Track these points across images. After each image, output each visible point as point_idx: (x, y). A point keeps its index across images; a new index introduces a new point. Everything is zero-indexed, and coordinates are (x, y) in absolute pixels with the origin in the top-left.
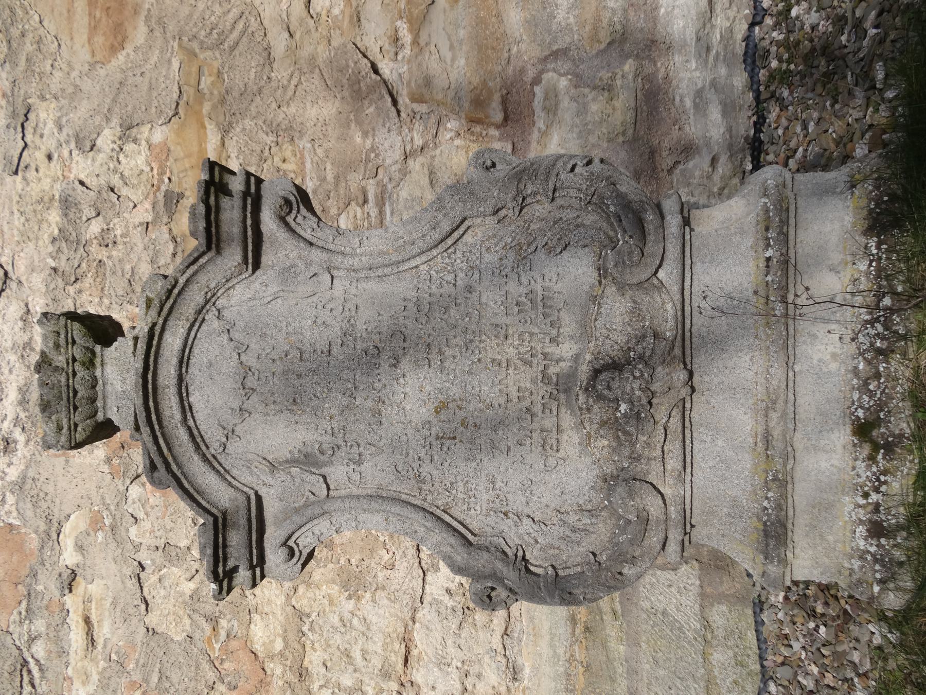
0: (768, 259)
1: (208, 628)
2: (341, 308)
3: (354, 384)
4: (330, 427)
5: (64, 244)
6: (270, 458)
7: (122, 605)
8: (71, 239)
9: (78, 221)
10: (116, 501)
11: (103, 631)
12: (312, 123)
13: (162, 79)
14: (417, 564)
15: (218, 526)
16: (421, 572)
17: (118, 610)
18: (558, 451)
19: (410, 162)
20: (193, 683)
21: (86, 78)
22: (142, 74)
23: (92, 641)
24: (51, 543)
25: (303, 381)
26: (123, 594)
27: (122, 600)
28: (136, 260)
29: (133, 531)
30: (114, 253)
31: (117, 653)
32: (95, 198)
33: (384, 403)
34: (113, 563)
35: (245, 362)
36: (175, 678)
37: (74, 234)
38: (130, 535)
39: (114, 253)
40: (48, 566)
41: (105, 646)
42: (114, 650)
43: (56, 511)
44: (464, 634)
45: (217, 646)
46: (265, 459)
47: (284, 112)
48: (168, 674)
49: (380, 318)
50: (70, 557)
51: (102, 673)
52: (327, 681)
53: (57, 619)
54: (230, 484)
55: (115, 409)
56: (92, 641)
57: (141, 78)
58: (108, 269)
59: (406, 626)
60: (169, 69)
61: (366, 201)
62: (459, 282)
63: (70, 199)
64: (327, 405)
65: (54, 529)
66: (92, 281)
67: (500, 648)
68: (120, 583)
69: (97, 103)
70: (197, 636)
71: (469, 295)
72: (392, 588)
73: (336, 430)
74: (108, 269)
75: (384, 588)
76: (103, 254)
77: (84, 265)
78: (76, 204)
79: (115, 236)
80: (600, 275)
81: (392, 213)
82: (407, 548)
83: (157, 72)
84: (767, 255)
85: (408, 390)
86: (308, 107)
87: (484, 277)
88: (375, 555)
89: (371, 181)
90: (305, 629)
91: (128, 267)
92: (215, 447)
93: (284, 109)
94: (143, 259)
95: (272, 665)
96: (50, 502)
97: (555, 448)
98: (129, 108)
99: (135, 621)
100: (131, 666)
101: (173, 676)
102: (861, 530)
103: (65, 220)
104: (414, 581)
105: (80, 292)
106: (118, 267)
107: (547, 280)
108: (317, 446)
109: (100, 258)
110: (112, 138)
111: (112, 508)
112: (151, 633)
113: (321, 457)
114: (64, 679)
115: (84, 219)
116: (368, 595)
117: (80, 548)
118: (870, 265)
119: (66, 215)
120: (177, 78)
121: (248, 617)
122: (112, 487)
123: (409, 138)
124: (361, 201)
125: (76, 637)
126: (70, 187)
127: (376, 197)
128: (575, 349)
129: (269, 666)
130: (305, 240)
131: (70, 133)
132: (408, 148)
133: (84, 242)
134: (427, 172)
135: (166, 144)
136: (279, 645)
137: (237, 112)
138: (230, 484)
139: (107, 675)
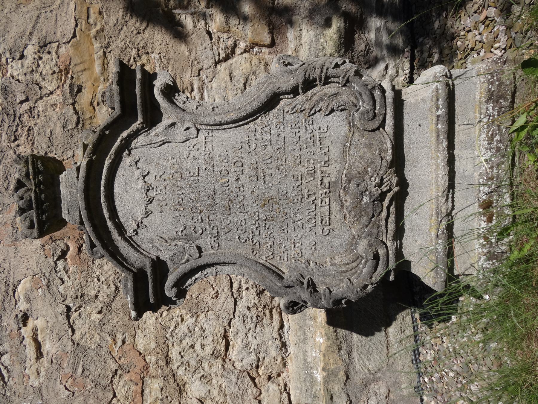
0: (438, 116)
1: (110, 339)
2: (204, 148)
3: (214, 191)
4: (200, 217)
5: (6, 117)
6: (164, 236)
7: (57, 331)
8: (10, 113)
9: (14, 102)
10: (49, 270)
11: (46, 347)
12: (159, 44)
13: (63, 15)
14: (230, 295)
15: (139, 277)
16: (233, 299)
17: (55, 333)
18: (330, 225)
19: (218, 66)
20: (103, 371)
21: (14, 13)
22: (51, 11)
23: (39, 355)
24: (9, 298)
25: (183, 191)
26: (56, 324)
27: (57, 328)
28: (53, 126)
29: (61, 288)
30: (38, 121)
31: (56, 358)
32: (24, 88)
33: (232, 202)
34: (49, 307)
35: (147, 181)
36: (92, 369)
37: (12, 111)
38: (60, 290)
39: (38, 121)
40: (8, 311)
41: (48, 355)
42: (54, 357)
43: (11, 278)
44: (258, 329)
45: (116, 350)
46: (161, 238)
47: (142, 37)
48: (88, 367)
49: (227, 153)
50: (23, 306)
51: (47, 370)
52: (182, 363)
53: (17, 341)
54: (141, 253)
55: (67, 212)
56: (39, 355)
57: (51, 14)
58: (35, 131)
59: (225, 329)
60: (68, 8)
61: (193, 90)
62: (272, 132)
63: (8, 89)
64: (198, 205)
65: (10, 289)
66: (25, 139)
67: (278, 337)
68: (55, 318)
69: (22, 29)
70: (104, 345)
71: (278, 139)
72: (217, 309)
73: (204, 219)
74: (35, 131)
75: (212, 310)
76: (31, 123)
77: (19, 129)
78: (12, 92)
79: (39, 112)
80: (350, 126)
81: (209, 97)
82: (224, 287)
83: (60, 10)
84: (438, 113)
85: (245, 194)
86: (156, 34)
87: (286, 129)
88: (206, 291)
89: (195, 78)
90: (168, 336)
91: (48, 131)
92: (130, 231)
93: (142, 34)
94: (58, 125)
95: (149, 357)
96: (7, 273)
97: (328, 223)
98: (44, 32)
99: (65, 339)
100: (65, 365)
101: (91, 368)
102: (483, 258)
103: (5, 102)
104: (229, 305)
105: (18, 146)
106: (42, 130)
107: (322, 129)
108: (193, 229)
109: (30, 125)
110: (33, 51)
111: (47, 275)
112: (76, 345)
113: (195, 235)
114: (24, 376)
115: (18, 101)
116: (203, 314)
117: (28, 300)
118: (489, 119)
119: (6, 99)
120: (74, 14)
121: (134, 332)
122: (46, 262)
123: (217, 53)
124: (190, 90)
125: (30, 352)
126: (7, 81)
127: (199, 88)
128: (338, 167)
129: (148, 358)
130: (180, 107)
131: (6, 48)
132: (217, 59)
133: (19, 115)
134: (228, 73)
135: (68, 55)
136: (153, 345)
137: (113, 36)
138: (141, 253)
139: (50, 372)
